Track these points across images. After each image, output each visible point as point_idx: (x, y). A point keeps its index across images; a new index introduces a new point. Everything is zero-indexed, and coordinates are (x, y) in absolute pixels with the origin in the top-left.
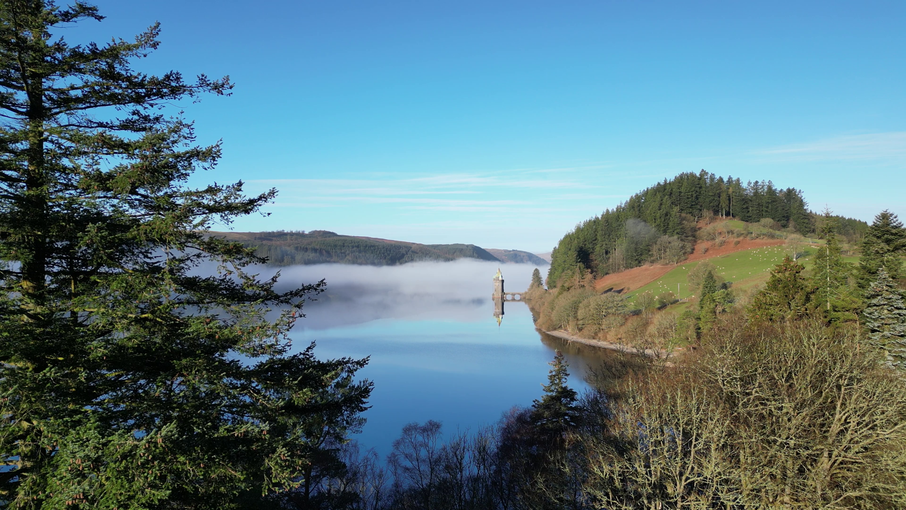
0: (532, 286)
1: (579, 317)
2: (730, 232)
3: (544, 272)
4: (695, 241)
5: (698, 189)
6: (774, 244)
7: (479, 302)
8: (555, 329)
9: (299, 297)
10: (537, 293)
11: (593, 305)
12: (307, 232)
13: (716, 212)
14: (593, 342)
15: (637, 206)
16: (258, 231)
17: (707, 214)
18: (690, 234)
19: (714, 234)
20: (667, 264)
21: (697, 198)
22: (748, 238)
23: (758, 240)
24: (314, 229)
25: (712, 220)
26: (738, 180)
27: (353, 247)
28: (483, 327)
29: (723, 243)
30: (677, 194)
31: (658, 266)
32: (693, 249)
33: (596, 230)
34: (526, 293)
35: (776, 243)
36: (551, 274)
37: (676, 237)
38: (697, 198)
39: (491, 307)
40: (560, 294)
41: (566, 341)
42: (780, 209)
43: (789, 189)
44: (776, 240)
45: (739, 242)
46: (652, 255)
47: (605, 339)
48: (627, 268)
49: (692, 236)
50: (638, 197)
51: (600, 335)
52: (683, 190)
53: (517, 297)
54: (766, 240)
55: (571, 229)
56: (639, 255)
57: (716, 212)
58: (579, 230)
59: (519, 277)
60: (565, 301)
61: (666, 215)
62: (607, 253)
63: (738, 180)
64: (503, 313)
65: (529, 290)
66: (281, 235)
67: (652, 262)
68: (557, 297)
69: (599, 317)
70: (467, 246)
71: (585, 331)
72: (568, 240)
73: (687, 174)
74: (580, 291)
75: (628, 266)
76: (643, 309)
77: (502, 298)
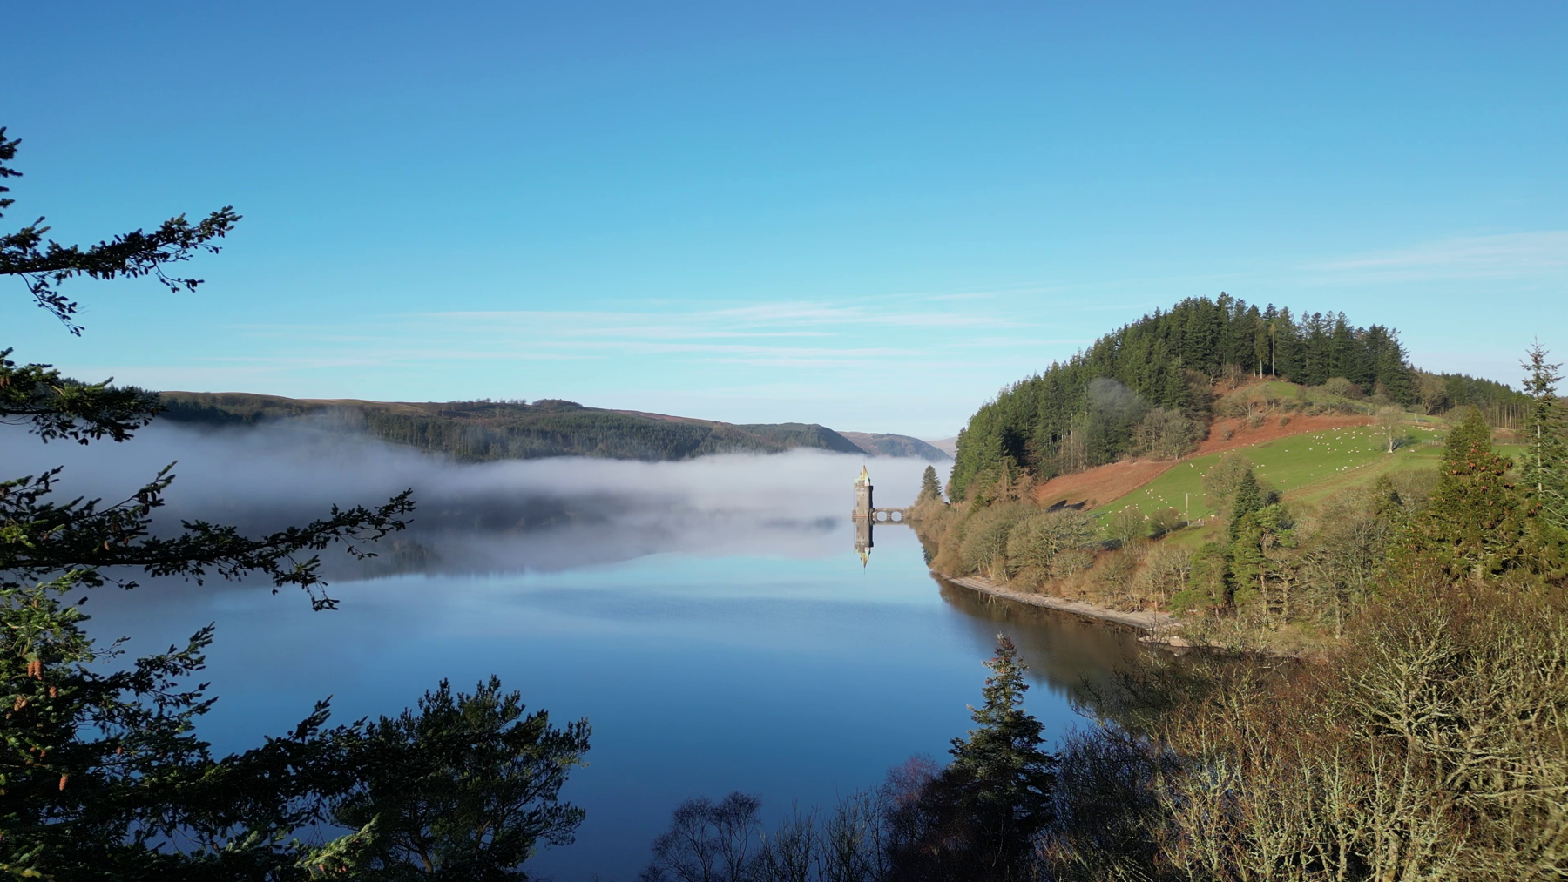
0: (922, 497)
1: (1010, 554)
2: (1273, 402)
3: (944, 472)
4: (1211, 419)
5: (1215, 327)
6: (1352, 423)
7: (828, 524)
8: (966, 575)
10: (932, 509)
11: (1035, 531)
12: (529, 403)
14: (1036, 598)
15: (1108, 357)
16: (445, 401)
17: (1232, 370)
20: (1161, 459)
21: (1213, 342)
22: (1305, 413)
23: (1322, 417)
25: (1241, 381)
26: (1286, 311)
29: (1260, 422)
31: (1145, 462)
32: (1208, 433)
34: (912, 509)
35: (1355, 422)
36: (956, 475)
37: (1177, 411)
38: (1213, 342)
39: (849, 533)
40: (974, 511)
42: (1361, 363)
44: (1355, 417)
45: (1288, 421)
46: (1135, 443)
47: (1058, 593)
48: (1090, 465)
49: (1203, 409)
50: (1109, 341)
52: (1188, 328)
53: (897, 516)
54: (1336, 416)
55: (992, 396)
56: (1111, 443)
57: (1247, 368)
58: (1005, 398)
59: (900, 482)
60: (983, 524)
61: (1160, 371)
62: (1055, 438)
63: (1286, 311)
64: (871, 545)
65: (918, 503)
66: (484, 407)
67: (1136, 455)
69: (1045, 555)
70: (809, 427)
71: (1021, 579)
72: (986, 416)
73: (1195, 301)
74: (1010, 505)
75: (1093, 463)
77: (870, 517)
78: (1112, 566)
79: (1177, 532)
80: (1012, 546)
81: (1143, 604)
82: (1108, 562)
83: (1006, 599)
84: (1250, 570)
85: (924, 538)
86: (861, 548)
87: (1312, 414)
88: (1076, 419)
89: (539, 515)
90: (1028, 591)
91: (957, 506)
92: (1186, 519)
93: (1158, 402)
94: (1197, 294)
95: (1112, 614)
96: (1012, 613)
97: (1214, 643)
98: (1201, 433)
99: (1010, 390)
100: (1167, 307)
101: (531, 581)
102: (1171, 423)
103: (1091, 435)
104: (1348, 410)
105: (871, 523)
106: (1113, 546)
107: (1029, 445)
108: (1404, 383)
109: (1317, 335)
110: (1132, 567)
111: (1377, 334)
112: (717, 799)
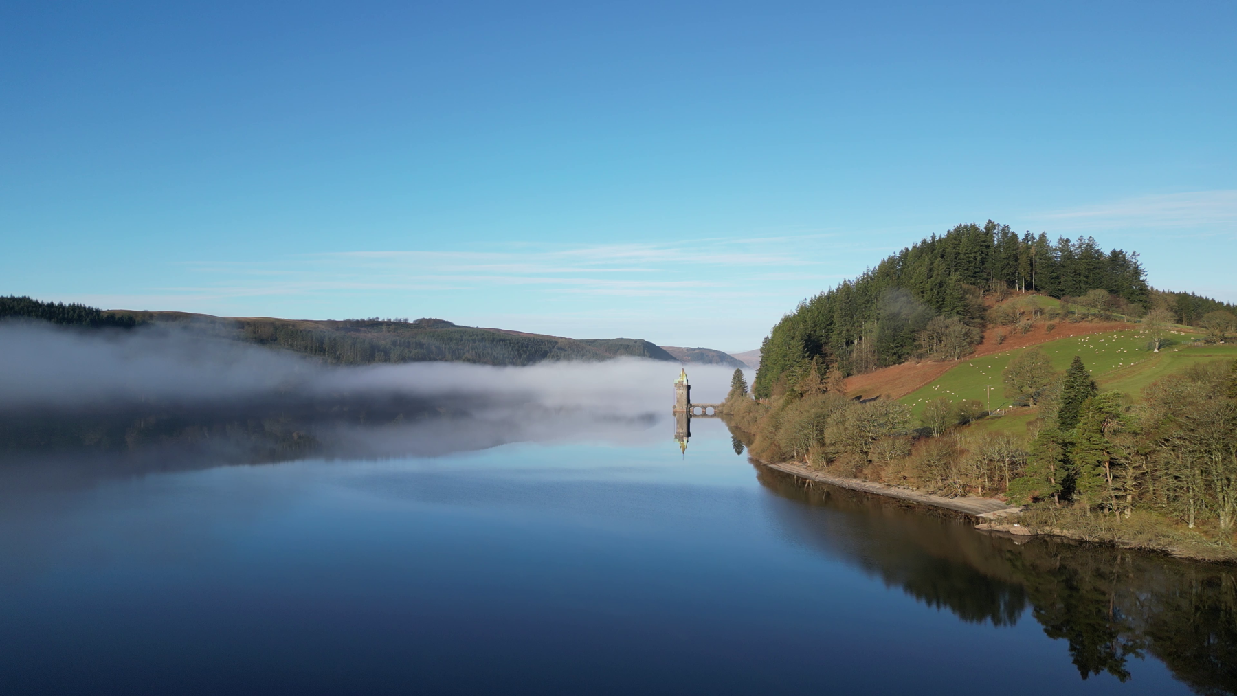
0: (732, 394)
1: (828, 441)
2: (1039, 311)
3: (750, 377)
4: (984, 326)
5: (983, 249)
6: (1112, 328)
7: (649, 419)
8: (784, 460)
10: (741, 405)
11: (851, 420)
12: (411, 321)
13: (1011, 283)
14: (855, 483)
15: (893, 272)
16: (341, 319)
17: (999, 286)
18: (977, 314)
20: (943, 360)
22: (1068, 320)
23: (1083, 324)
24: (421, 317)
25: (1006, 295)
26: (1043, 236)
27: (474, 341)
28: (659, 457)
29: (1028, 329)
30: (953, 256)
31: (929, 363)
32: (983, 338)
34: (723, 405)
35: (1115, 328)
36: (760, 377)
37: (956, 318)
39: (670, 426)
40: (788, 402)
41: (802, 480)
42: (1102, 279)
43: (1114, 252)
44: (1113, 323)
45: (1052, 327)
46: (920, 346)
47: (878, 478)
48: (879, 366)
49: (978, 318)
50: (892, 260)
51: (867, 471)
52: (961, 249)
53: (710, 411)
54: (1096, 323)
55: (792, 309)
56: (897, 346)
57: (1011, 283)
58: (803, 310)
59: (713, 384)
60: (798, 415)
61: (941, 285)
62: (848, 343)
63: (1043, 236)
64: (689, 435)
65: (728, 400)
66: (374, 324)
67: (920, 357)
68: (784, 408)
69: (862, 443)
70: (636, 341)
71: (840, 464)
72: (787, 327)
73: (966, 227)
74: (821, 397)
75: (883, 364)
76: (935, 427)
77: (688, 412)
78: (934, 453)
79: (980, 421)
80: (828, 433)
81: (967, 490)
82: (924, 451)
83: (824, 483)
84: (1092, 458)
85: (735, 430)
87: (1075, 321)
88: (867, 326)
90: (847, 476)
91: (764, 402)
92: (988, 408)
93: (939, 310)
95: (935, 499)
96: (830, 497)
97: (1057, 531)
98: (977, 338)
100: (941, 233)
101: (362, 468)
102: (952, 329)
103: (880, 340)
104: (1108, 318)
106: (924, 434)
107: (826, 349)
108: (1143, 297)
109: (1068, 255)
110: (954, 453)
111: (1117, 256)
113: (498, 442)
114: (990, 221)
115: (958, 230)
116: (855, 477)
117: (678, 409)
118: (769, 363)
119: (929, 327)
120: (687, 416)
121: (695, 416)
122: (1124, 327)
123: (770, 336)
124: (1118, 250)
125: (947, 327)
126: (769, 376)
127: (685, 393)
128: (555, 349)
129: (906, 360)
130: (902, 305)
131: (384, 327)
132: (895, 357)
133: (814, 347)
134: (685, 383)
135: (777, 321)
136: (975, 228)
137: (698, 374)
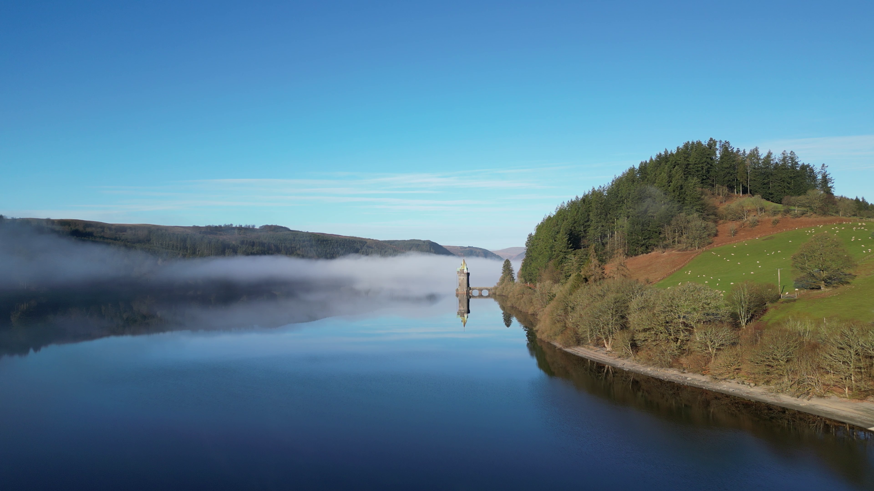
0: (503, 280)
3: (517, 266)
6: (831, 222)
7: (432, 298)
9: (228, 294)
12: (257, 227)
13: (731, 188)
14: (671, 374)
19: (743, 211)
21: (708, 172)
23: (803, 218)
25: (728, 197)
29: (755, 224)
33: (588, 211)
34: (496, 288)
36: (525, 266)
37: (696, 215)
38: (708, 172)
39: (454, 304)
40: (575, 287)
45: (776, 222)
47: (703, 371)
53: (485, 293)
56: (645, 239)
57: (731, 188)
59: (487, 274)
64: (469, 312)
67: (665, 247)
70: (424, 242)
72: (548, 226)
75: (631, 253)
77: (468, 294)
80: (634, 319)
86: (461, 314)
87: (796, 216)
89: (228, 294)
93: (680, 209)
94: (693, 138)
99: (566, 205)
102: (693, 224)
105: (469, 297)
112: (420, 290)
113: (312, 318)
114: (711, 139)
115: (686, 145)
116: (671, 367)
117: (460, 291)
118: (535, 254)
119: (673, 222)
120: (467, 297)
121: (474, 297)
122: (842, 221)
123: (534, 233)
124: (806, 164)
125: (688, 222)
126: (533, 264)
127: (466, 278)
128: (365, 247)
129: (653, 250)
130: (658, 203)
131: (236, 231)
132: (644, 248)
133: (575, 241)
134: (465, 271)
135: (539, 221)
136: (699, 143)
137: (474, 265)
